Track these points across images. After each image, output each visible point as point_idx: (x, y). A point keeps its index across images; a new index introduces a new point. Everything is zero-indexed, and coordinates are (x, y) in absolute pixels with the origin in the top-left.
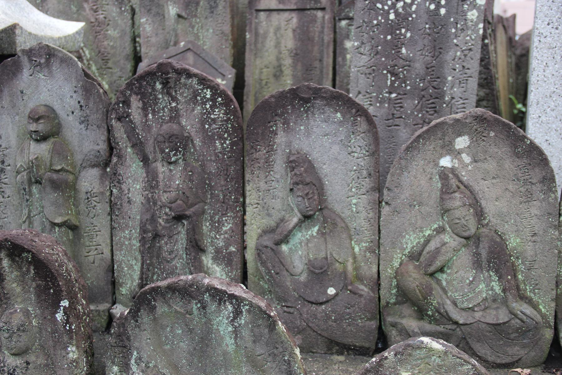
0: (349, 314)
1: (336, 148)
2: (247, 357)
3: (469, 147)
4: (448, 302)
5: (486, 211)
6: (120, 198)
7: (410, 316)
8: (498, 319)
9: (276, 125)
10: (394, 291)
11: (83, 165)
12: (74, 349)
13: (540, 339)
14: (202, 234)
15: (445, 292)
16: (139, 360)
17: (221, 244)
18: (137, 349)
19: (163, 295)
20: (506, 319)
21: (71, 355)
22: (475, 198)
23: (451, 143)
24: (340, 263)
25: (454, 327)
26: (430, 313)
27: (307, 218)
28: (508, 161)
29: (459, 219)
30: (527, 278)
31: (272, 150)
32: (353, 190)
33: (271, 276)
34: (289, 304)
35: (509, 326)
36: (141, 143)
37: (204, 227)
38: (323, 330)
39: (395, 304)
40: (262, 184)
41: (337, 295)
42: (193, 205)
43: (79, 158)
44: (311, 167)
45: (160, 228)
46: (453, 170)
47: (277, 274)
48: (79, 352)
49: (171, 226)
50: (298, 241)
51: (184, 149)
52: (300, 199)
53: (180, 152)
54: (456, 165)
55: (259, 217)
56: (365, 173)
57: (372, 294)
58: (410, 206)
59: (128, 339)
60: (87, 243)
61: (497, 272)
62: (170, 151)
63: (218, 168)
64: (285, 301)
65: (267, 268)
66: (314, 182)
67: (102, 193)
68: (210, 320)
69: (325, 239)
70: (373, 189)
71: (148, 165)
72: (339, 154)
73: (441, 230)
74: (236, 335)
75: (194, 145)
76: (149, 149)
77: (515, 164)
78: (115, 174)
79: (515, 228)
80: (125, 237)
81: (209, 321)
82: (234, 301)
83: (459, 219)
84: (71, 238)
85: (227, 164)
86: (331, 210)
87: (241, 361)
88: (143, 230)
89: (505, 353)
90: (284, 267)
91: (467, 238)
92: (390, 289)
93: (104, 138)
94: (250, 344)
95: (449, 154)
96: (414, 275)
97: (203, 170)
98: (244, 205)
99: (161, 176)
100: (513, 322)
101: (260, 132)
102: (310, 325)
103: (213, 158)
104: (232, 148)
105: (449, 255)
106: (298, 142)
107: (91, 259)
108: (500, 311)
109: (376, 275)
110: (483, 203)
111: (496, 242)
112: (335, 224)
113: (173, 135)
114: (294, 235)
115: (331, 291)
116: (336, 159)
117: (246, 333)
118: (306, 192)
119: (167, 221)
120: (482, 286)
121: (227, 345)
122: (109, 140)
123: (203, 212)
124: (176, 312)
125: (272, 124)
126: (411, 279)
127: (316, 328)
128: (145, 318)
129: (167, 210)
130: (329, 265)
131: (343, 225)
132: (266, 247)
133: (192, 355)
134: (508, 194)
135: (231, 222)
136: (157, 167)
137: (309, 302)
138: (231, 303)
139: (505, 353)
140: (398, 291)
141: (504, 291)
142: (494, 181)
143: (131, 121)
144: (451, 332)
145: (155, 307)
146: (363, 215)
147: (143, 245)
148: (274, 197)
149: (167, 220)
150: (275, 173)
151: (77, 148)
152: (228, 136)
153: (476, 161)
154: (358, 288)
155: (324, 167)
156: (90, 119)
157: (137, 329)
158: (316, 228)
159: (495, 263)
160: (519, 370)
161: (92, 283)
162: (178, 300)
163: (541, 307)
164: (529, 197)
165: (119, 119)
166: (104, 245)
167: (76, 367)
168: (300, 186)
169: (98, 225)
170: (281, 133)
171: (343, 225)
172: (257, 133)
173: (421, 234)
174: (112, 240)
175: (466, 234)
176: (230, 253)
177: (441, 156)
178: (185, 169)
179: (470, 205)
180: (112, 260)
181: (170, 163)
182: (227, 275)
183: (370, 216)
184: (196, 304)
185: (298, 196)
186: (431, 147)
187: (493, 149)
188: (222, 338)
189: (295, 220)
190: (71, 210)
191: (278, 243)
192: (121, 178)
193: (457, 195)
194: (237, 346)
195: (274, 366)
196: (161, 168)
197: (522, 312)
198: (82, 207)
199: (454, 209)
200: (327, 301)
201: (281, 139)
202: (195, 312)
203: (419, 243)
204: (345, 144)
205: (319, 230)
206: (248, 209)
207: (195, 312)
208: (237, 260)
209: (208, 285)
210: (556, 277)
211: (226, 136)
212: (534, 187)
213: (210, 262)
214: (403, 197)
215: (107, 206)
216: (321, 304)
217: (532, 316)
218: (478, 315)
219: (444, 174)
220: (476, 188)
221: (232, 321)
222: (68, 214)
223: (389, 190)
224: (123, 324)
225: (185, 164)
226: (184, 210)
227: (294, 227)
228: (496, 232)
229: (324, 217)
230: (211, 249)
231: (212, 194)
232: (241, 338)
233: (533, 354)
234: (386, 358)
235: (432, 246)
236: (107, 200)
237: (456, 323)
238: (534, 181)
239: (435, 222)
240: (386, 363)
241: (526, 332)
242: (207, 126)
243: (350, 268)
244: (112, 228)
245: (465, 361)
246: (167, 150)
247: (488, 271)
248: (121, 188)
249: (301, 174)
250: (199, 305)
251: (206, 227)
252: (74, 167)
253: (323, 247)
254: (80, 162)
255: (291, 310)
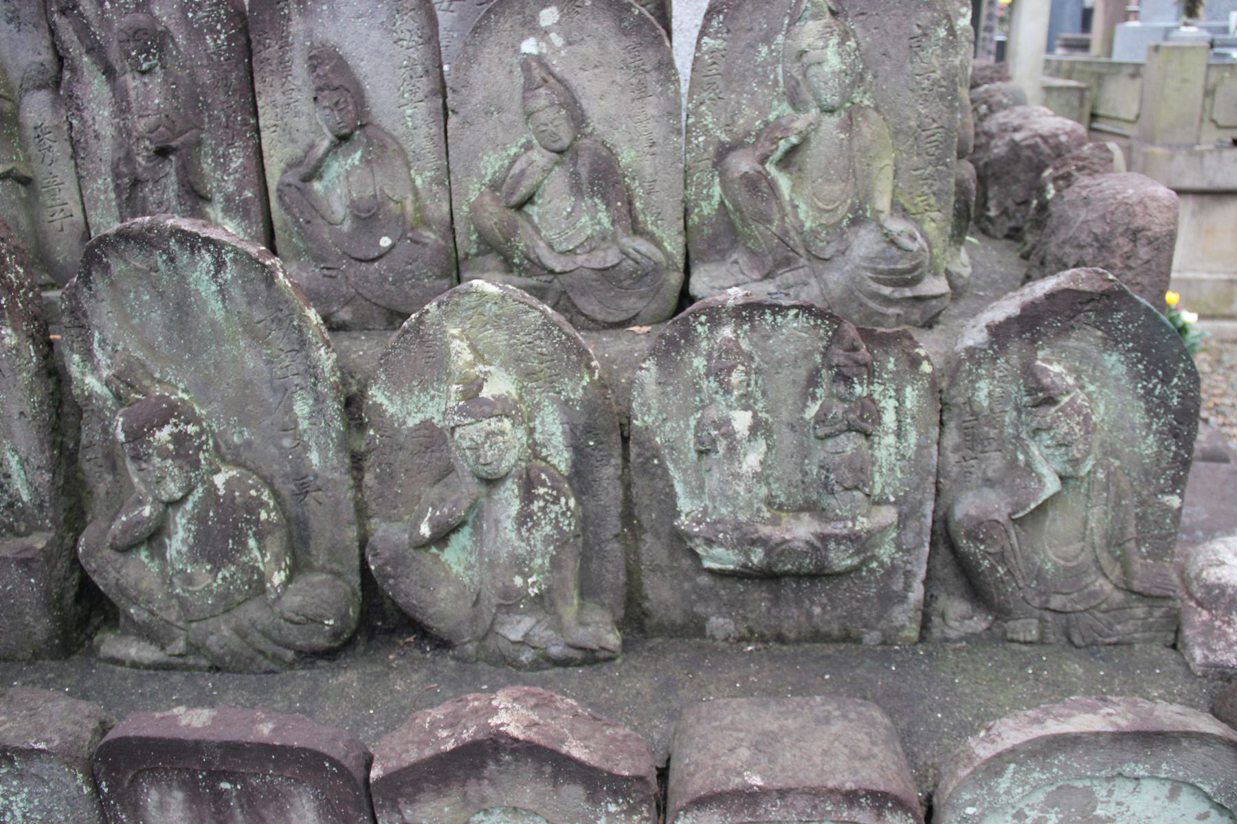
0: (411, 271)
1: (376, 35)
2: (244, 326)
3: (558, 23)
4: (542, 244)
5: (589, 114)
6: (82, 132)
7: (495, 269)
8: (605, 262)
9: (288, 5)
10: (474, 237)
11: (24, 86)
12: (9, 331)
13: (662, 285)
14: (202, 176)
15: (538, 231)
16: (103, 341)
17: (231, 188)
18: (98, 327)
19: (114, 247)
20: (616, 261)
21: (7, 340)
22: (573, 97)
23: (534, 18)
24: (397, 202)
25: (550, 277)
26: (516, 261)
27: (343, 139)
28: (612, 41)
29: (546, 125)
30: (647, 205)
31: (287, 44)
32: (406, 95)
33: (300, 227)
34: (329, 265)
35: (620, 271)
36: (101, 47)
37: (205, 166)
38: (378, 297)
39: (477, 255)
40: (278, 96)
41: (393, 246)
42: (181, 133)
43: (15, 76)
44: (341, 65)
45: (140, 170)
46: (539, 59)
47: (308, 222)
48: (17, 335)
49: (154, 166)
50: (334, 175)
51: (161, 51)
52: (328, 111)
53: (154, 55)
54: (544, 51)
55: (279, 145)
56: (420, 69)
57: (442, 243)
58: (486, 113)
59: (85, 314)
60: (49, 203)
61: (603, 197)
62: (139, 54)
63: (214, 77)
64: (324, 260)
65: (294, 216)
66: (347, 85)
67: (57, 127)
68: (184, 278)
69: (372, 170)
70: (433, 93)
71: (115, 79)
72: (381, 43)
73: (528, 147)
74: (224, 296)
75: (175, 44)
76: (114, 55)
77: (622, 44)
78: (70, 97)
79: (628, 137)
80: (99, 190)
81: (183, 280)
82: (212, 248)
83: (546, 125)
84: (24, 195)
85: (225, 71)
86: (378, 127)
87: (236, 333)
88: (117, 176)
89: (618, 308)
90: (317, 211)
91: (560, 152)
92: (468, 234)
93: (46, 42)
94: (244, 308)
95: (532, 34)
96: (491, 209)
97: (193, 81)
98: (257, 130)
99: (133, 94)
100: (624, 264)
101: (267, 18)
102: (361, 291)
103: (205, 62)
104: (229, 45)
105: (538, 177)
106: (321, 29)
107: (57, 224)
108: (610, 252)
109: (448, 217)
110: (584, 103)
111: (600, 157)
112: (384, 147)
113: (139, 30)
114: (328, 166)
115: (385, 242)
116: (378, 51)
117: (235, 292)
118: (334, 100)
119: (148, 159)
120: (585, 219)
121: (213, 311)
122: (54, 45)
123: (199, 143)
124: (137, 269)
125: (282, 4)
126: (487, 214)
127: (369, 295)
128: (100, 283)
129: (147, 143)
130: (380, 206)
131: (396, 147)
132: (289, 185)
133: (169, 328)
134: (616, 89)
135: (242, 154)
136: (125, 81)
137: (357, 259)
138: (209, 251)
139: (618, 308)
140: (479, 236)
141: (613, 223)
142: (597, 71)
143: (81, 15)
144: (546, 285)
145: (109, 266)
146: (423, 130)
147: (119, 196)
148: (297, 114)
149: (148, 157)
150: (295, 78)
151: (9, 61)
152: (223, 26)
153: (570, 43)
154: (421, 235)
155: (362, 64)
156: (21, 14)
157: (93, 301)
158: (358, 155)
159: (600, 185)
160: (636, 329)
161: (65, 258)
162: (136, 251)
163: (666, 244)
164: (642, 91)
165: (63, 12)
166: (71, 203)
167: (17, 356)
168: (326, 92)
169: (60, 174)
170: (296, 18)
171: (396, 147)
172: (264, 21)
173: (505, 154)
174: (82, 196)
175: (557, 146)
176: (246, 201)
177: (523, 38)
178: (165, 81)
179: (561, 105)
180: (87, 224)
181: (143, 73)
182: (245, 232)
183: (432, 131)
184: (161, 255)
185: (325, 107)
186: (507, 26)
187: (591, 25)
188: (205, 302)
189: (326, 144)
190: (17, 154)
191: (308, 178)
192: (79, 102)
193: (542, 91)
194: (227, 311)
195: (281, 335)
196: (132, 82)
197: (635, 250)
198: (33, 149)
199: (539, 111)
200: (380, 257)
201: (297, 26)
202: (162, 267)
203: (502, 166)
204: (388, 28)
205: (362, 157)
206: (263, 134)
207: (162, 267)
208: (255, 209)
209: (172, 227)
210: (683, 201)
211: (219, 27)
212: (648, 77)
213: (220, 215)
214: (474, 101)
215: (67, 144)
216: (373, 260)
217: (649, 254)
218: (580, 260)
219: (526, 66)
220: (574, 82)
221: (215, 276)
222: (12, 160)
223: (454, 91)
224: (74, 295)
225: (165, 74)
226: (168, 140)
227: (326, 154)
228: (603, 143)
229: (367, 137)
230: (218, 197)
231: (210, 116)
232: (231, 299)
233: (654, 306)
234: (427, 312)
235: (516, 169)
236: (66, 137)
237: (552, 272)
238: (648, 68)
239: (521, 135)
240: (428, 319)
241: (642, 276)
242: (190, 15)
243: (409, 208)
244: (80, 178)
245: (530, 306)
246: (134, 53)
247: (592, 197)
248: (82, 118)
249: (325, 75)
250: (165, 257)
251: (207, 165)
252: (11, 91)
253: (369, 181)
254: (18, 83)
255: (333, 273)
